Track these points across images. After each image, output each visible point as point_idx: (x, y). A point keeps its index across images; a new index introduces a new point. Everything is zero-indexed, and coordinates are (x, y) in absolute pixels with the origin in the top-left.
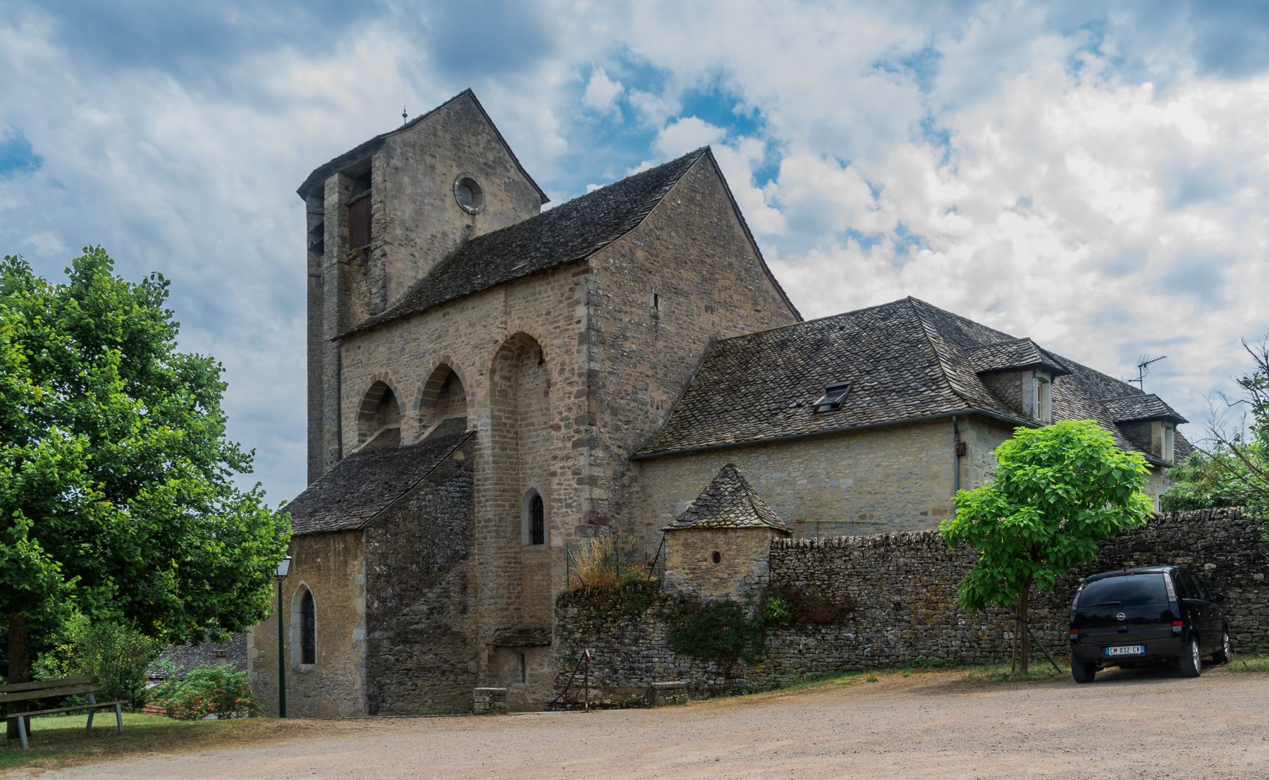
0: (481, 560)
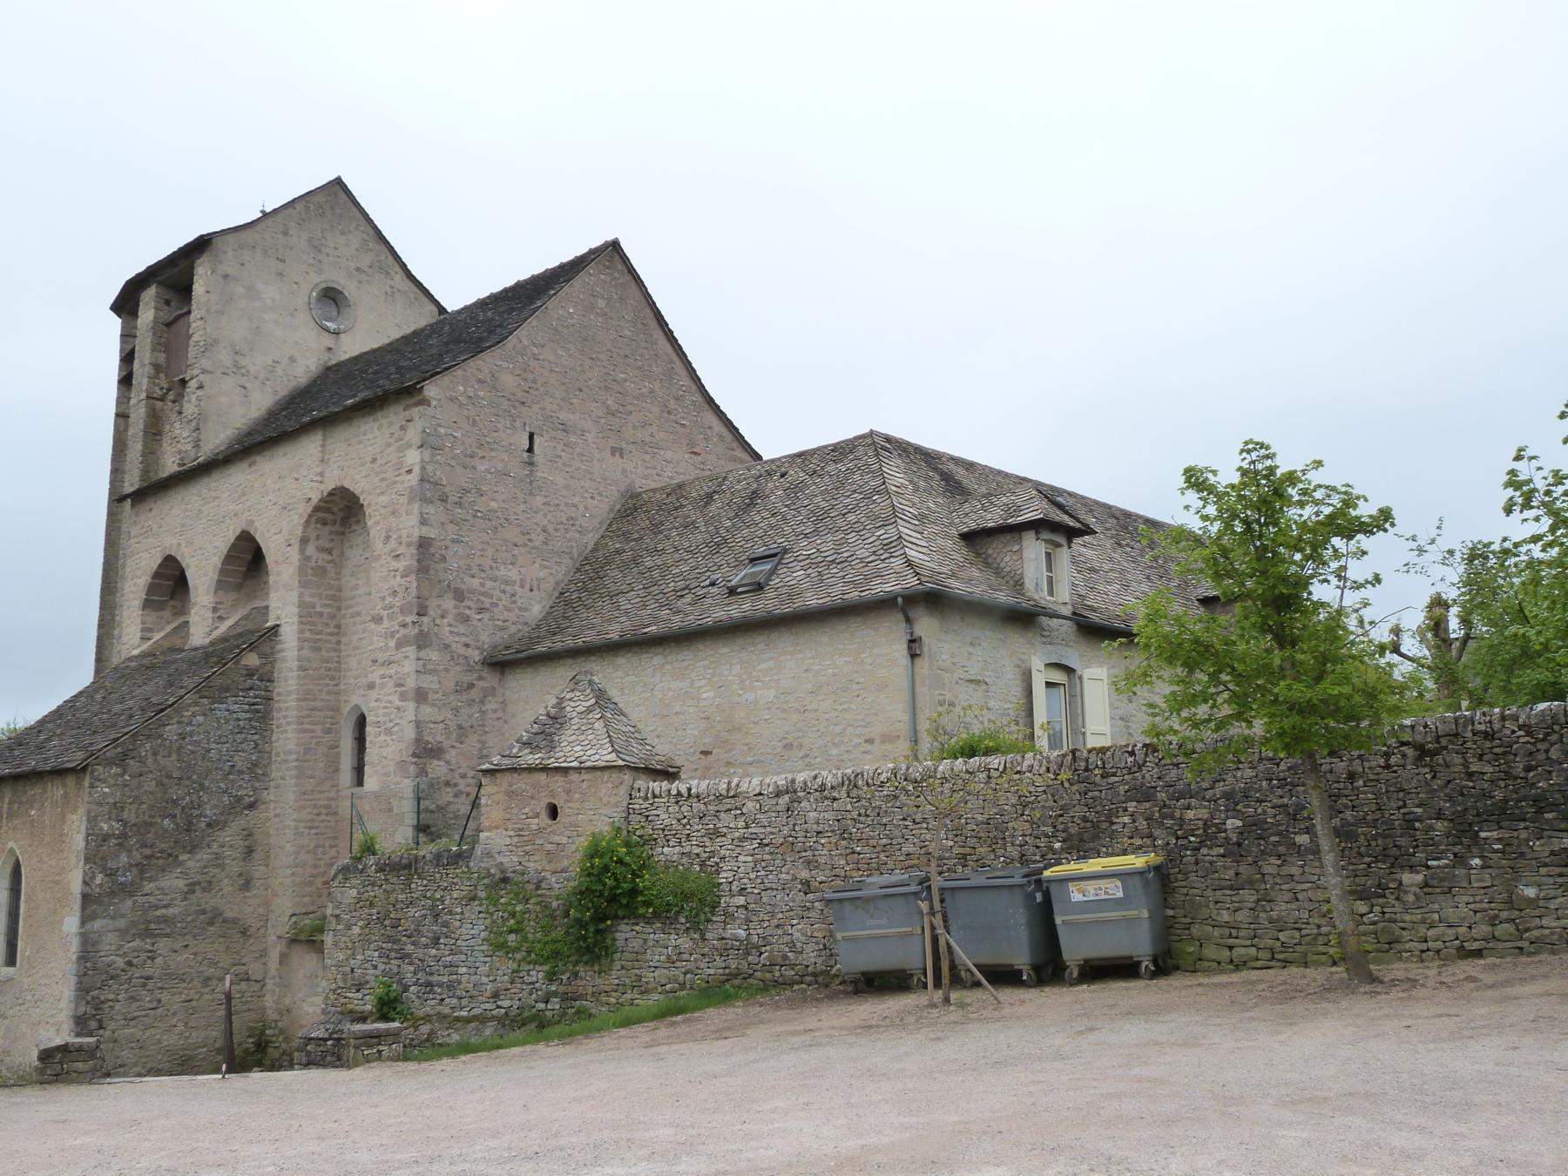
0: (278, 811)
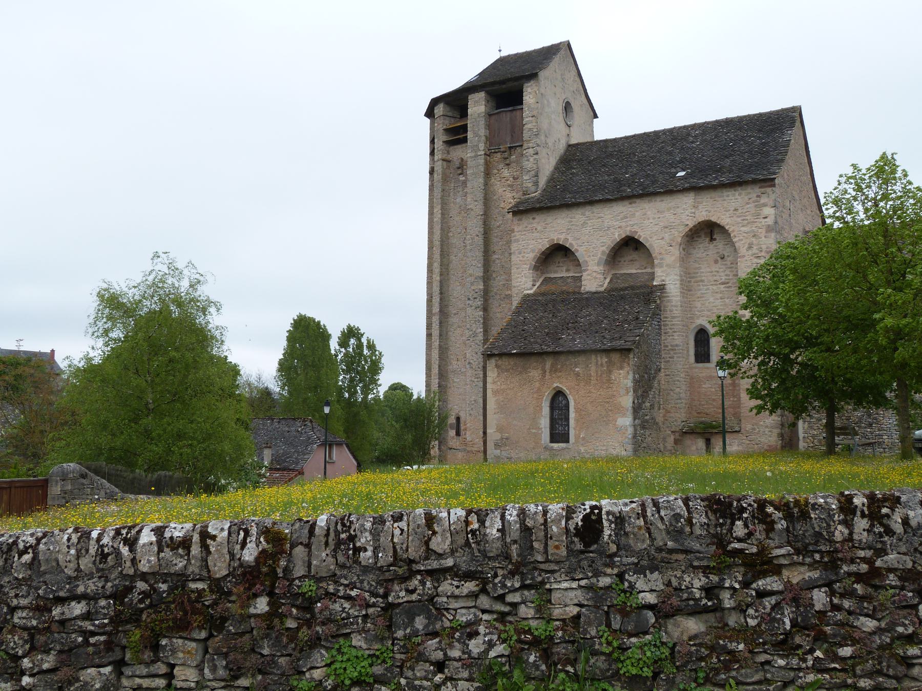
0: (667, 373)
